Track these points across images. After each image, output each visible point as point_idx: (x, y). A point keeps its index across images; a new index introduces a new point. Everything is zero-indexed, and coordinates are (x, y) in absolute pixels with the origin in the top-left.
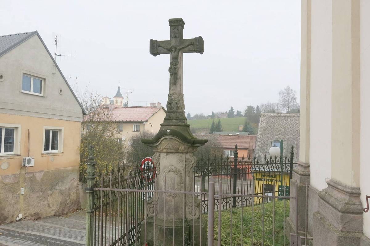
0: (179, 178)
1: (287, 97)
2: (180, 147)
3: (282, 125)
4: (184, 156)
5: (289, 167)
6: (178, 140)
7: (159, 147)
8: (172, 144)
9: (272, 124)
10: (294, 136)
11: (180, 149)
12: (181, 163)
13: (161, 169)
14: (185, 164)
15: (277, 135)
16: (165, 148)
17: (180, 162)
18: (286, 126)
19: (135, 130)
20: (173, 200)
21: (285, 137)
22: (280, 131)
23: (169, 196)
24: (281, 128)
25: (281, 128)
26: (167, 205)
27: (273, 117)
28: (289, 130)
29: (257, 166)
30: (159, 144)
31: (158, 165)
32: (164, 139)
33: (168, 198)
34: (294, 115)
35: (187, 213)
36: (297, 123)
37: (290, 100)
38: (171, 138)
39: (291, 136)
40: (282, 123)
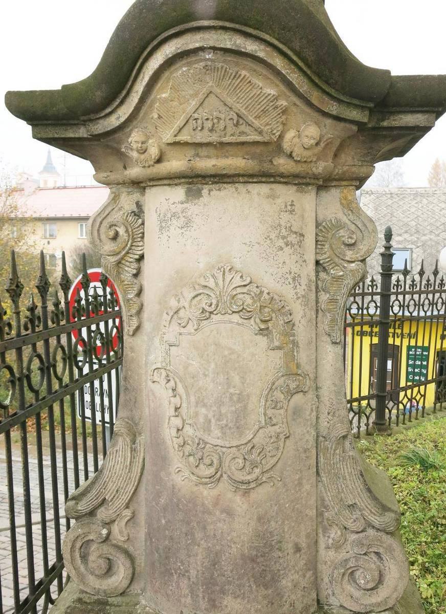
0: (280, 353)
1: (385, 172)
2: (290, 135)
3: (409, 212)
4: (307, 201)
5: (376, 307)
6: (278, 62)
7: (135, 137)
8: (230, 101)
9: (388, 211)
10: (438, 235)
11: (286, 145)
12: (287, 250)
13: (150, 297)
14: (311, 258)
15: (400, 235)
16: (175, 144)
17: (281, 243)
18: (419, 214)
19: (82, 235)
20: (239, 503)
21: (418, 238)
22: (407, 224)
23: (215, 479)
24: (409, 219)
25: (409, 219)
26: (199, 535)
27: (389, 196)
28: (426, 224)
29: (372, 300)
30: (138, 109)
31: (130, 269)
32: (169, 63)
33: (207, 494)
34: (436, 191)
35: (325, 572)
36: (443, 209)
37: (392, 177)
38: (226, 51)
39: (432, 237)
40: (409, 207)
